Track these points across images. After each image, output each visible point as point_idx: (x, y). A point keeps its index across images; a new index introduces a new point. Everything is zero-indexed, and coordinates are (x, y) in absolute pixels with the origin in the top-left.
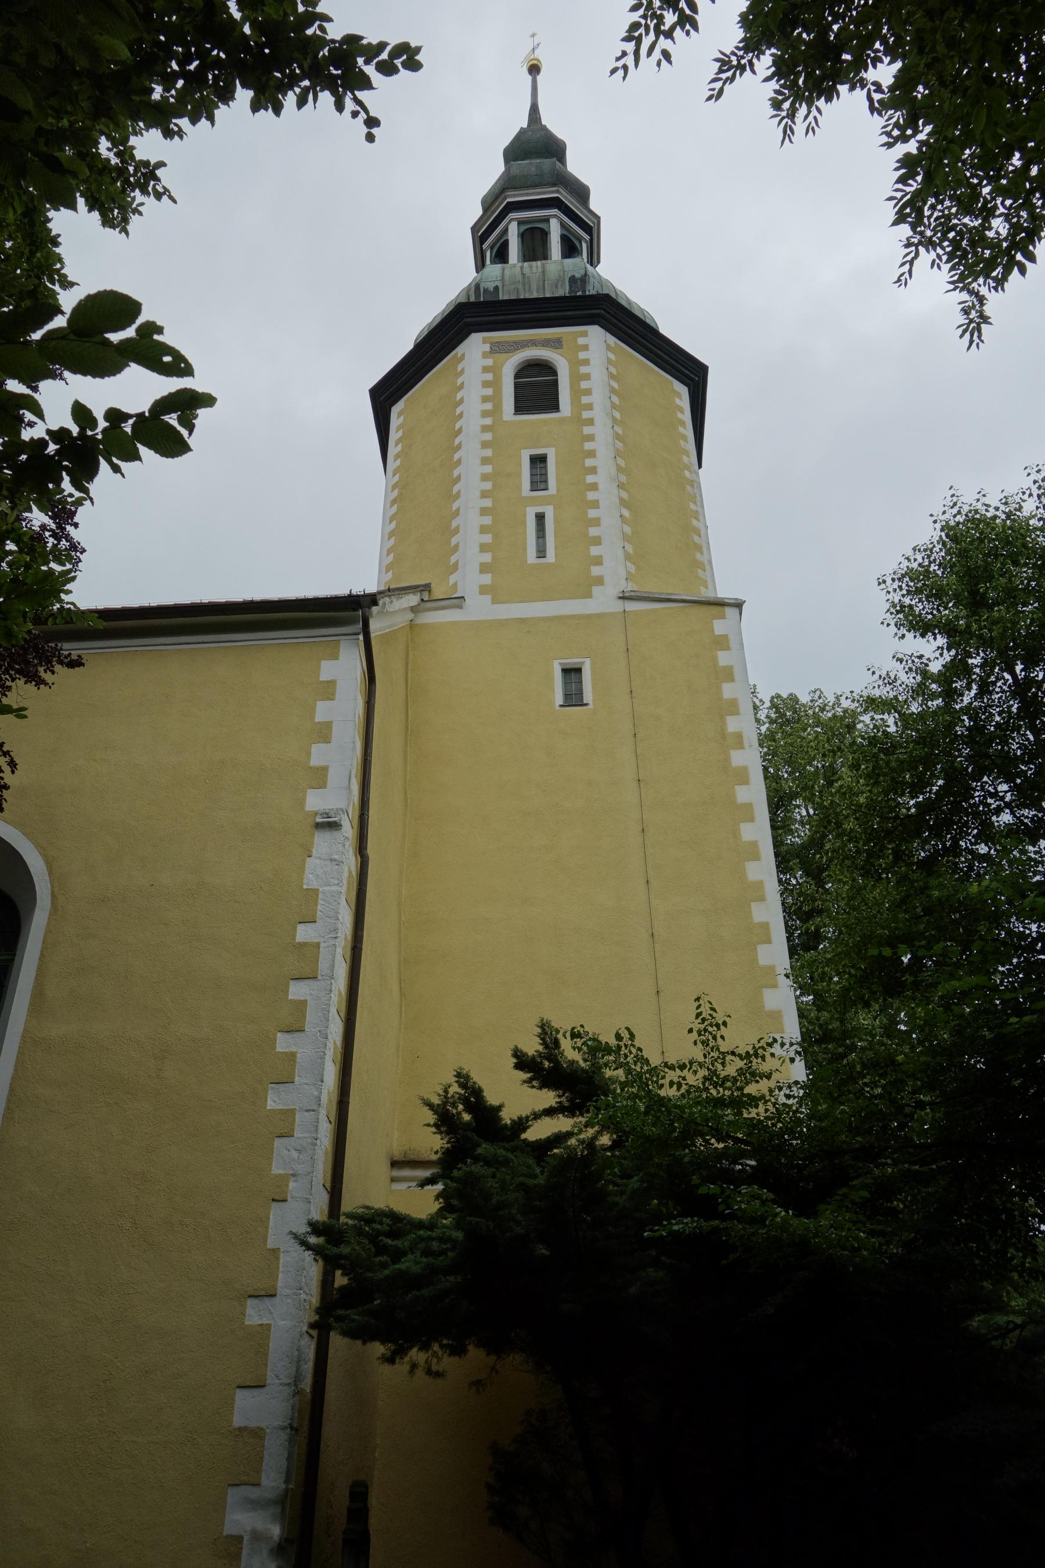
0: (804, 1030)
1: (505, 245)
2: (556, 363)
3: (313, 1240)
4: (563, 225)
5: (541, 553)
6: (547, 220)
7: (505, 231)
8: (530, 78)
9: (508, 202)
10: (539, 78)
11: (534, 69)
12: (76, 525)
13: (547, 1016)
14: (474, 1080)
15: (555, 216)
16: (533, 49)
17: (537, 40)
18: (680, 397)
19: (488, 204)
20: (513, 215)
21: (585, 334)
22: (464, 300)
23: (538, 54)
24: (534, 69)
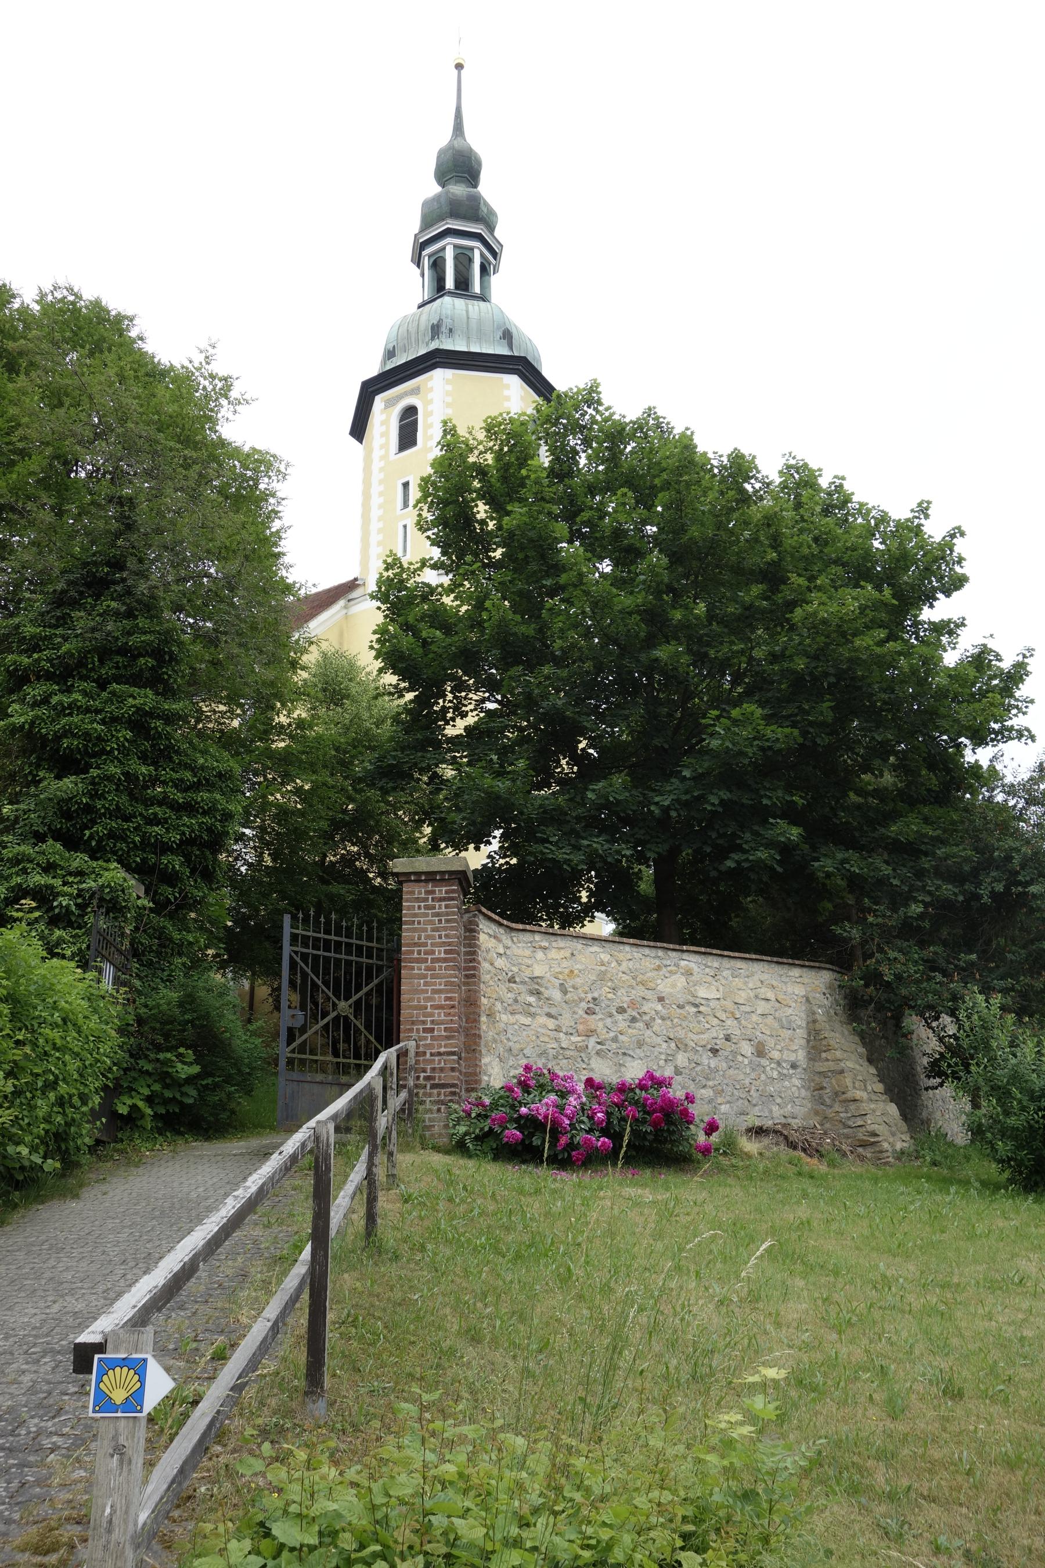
6: (443, 249)
8: (475, 140)
11: (459, 67)
20: (424, 253)
24: (459, 67)
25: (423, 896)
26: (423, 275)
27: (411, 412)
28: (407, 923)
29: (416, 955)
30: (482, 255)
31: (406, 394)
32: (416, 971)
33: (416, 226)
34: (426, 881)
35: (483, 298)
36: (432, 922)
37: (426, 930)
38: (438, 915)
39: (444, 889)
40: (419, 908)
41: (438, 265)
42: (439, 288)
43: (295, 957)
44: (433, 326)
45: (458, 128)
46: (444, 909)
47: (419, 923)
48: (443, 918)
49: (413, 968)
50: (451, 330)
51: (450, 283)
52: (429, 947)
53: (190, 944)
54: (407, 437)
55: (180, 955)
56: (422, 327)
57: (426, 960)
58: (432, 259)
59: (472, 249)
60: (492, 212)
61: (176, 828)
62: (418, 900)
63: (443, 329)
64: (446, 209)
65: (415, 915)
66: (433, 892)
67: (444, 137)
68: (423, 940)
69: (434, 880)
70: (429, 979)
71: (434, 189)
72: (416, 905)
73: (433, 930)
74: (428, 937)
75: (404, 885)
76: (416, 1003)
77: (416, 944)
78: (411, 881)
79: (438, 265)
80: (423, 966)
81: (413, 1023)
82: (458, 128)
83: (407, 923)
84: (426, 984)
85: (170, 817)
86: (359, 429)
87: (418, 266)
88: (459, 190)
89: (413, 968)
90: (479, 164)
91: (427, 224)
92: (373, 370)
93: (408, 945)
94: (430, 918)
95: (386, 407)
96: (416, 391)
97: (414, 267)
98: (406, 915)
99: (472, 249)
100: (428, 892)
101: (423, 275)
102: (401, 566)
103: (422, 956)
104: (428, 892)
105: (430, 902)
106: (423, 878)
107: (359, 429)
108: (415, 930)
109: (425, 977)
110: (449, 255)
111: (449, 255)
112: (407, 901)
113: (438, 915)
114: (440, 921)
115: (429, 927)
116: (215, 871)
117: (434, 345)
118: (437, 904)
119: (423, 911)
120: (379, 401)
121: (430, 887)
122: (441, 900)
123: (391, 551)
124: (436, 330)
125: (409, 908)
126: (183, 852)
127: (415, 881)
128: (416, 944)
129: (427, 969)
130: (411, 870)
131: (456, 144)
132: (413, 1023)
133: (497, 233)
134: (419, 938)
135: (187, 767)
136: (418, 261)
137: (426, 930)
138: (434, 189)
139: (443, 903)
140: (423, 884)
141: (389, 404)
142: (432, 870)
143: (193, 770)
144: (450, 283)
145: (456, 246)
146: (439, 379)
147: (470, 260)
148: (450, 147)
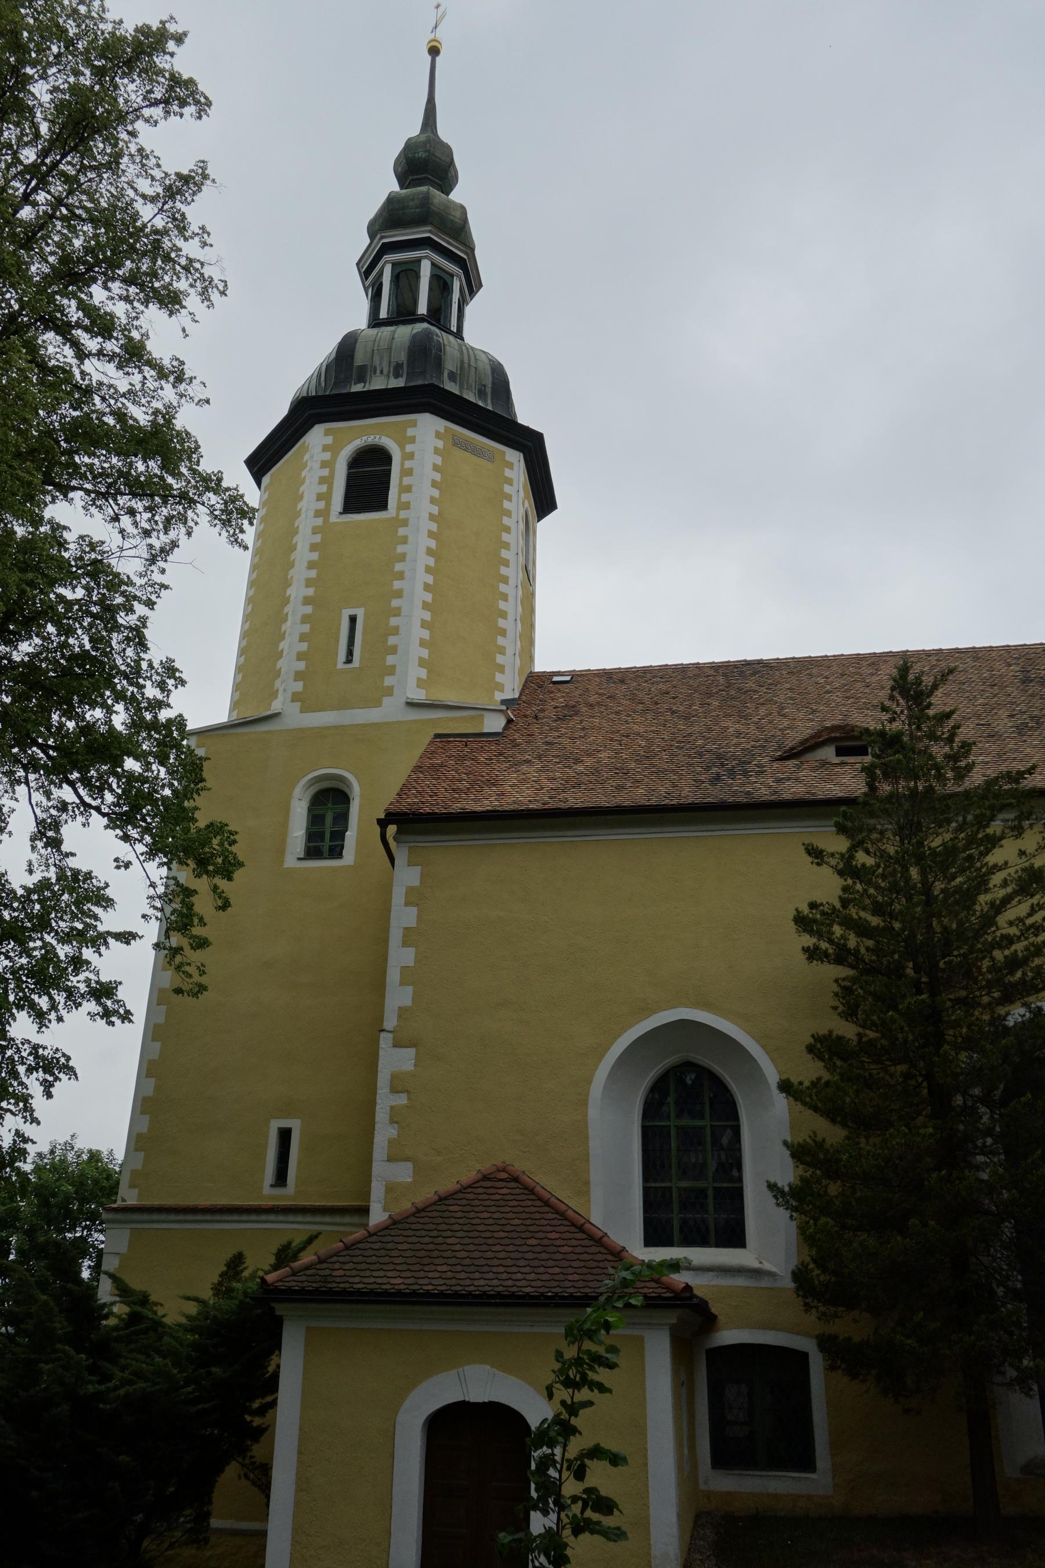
0: (735, 1173)
1: (381, 284)
2: (392, 453)
3: (106, 1310)
4: (433, 264)
5: (349, 660)
6: (418, 261)
7: (381, 274)
8: (429, 58)
9: (383, 243)
10: (438, 59)
11: (434, 51)
12: (1038, 843)
13: (594, 1407)
14: (84, 870)
15: (426, 257)
16: (436, 27)
17: (441, 10)
18: (511, 466)
19: (375, 229)
20: (387, 257)
21: (414, 424)
22: (305, 394)
23: (439, 34)
24: (434, 51)
35: (459, 335)
67: (414, 129)
110: (426, 270)
111: (426, 270)
120: (317, 437)
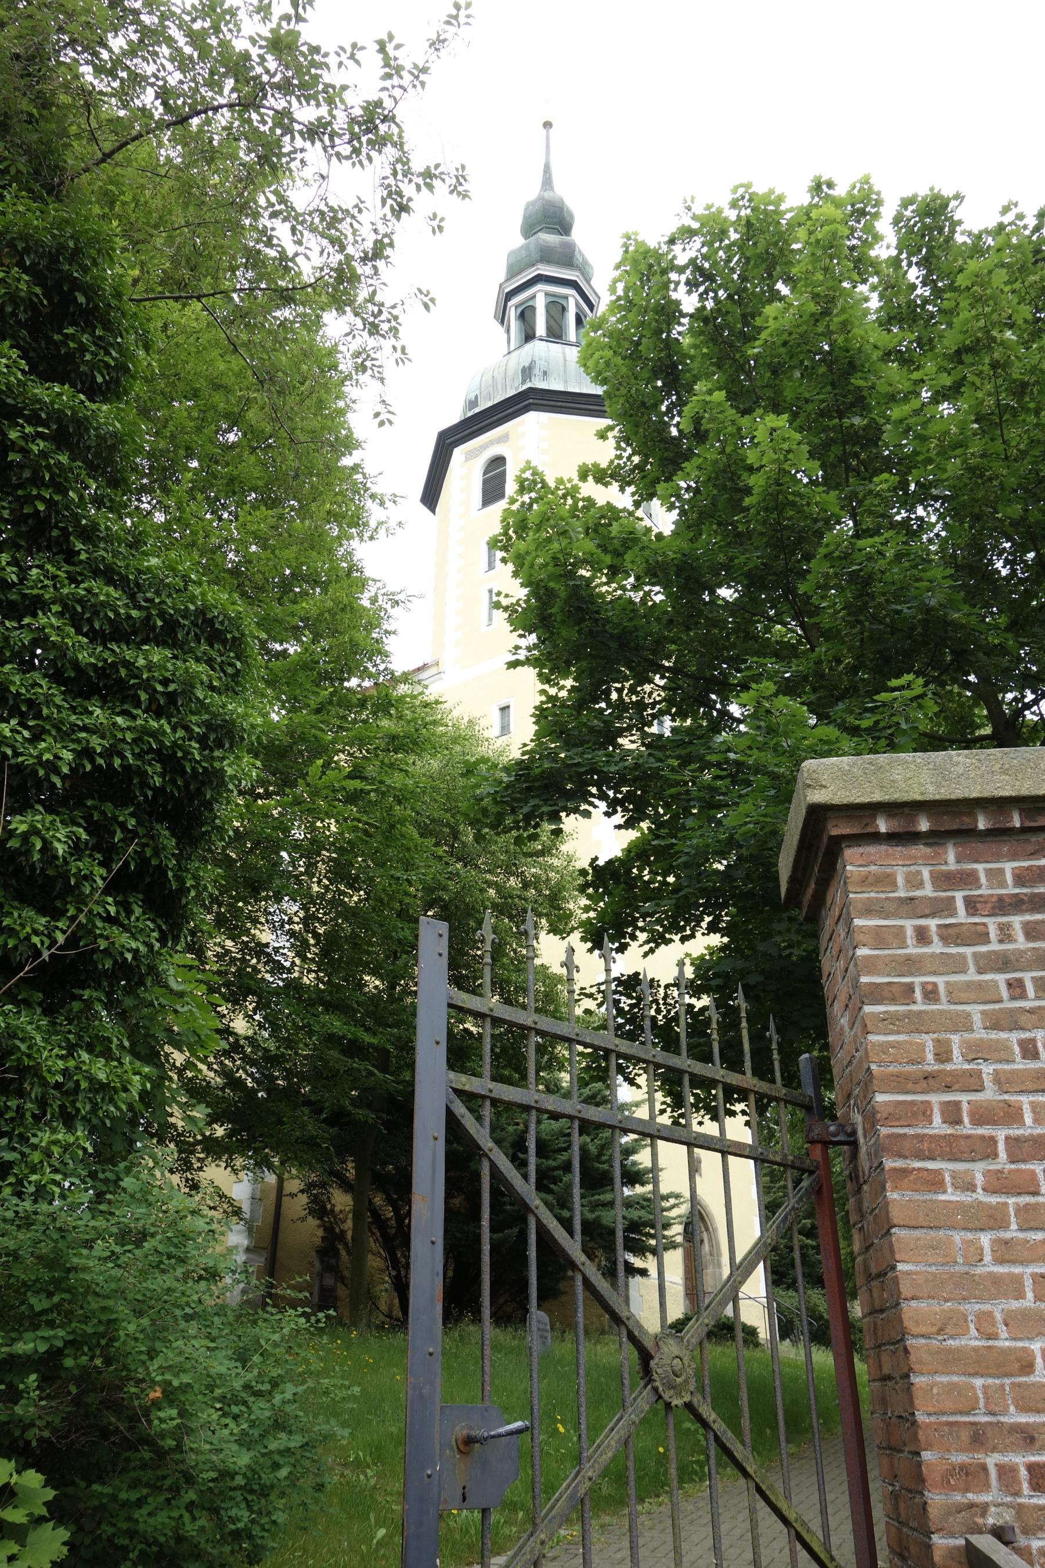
6: (533, 297)
11: (547, 125)
20: (510, 304)
25: (928, 891)
26: (508, 331)
27: (499, 461)
28: (877, 994)
29: (938, 1126)
30: (577, 305)
31: (491, 443)
32: (951, 1196)
33: (502, 276)
34: (935, 838)
36: (983, 993)
37: (963, 1024)
38: (1003, 963)
39: (1009, 867)
40: (922, 936)
41: (526, 315)
42: (529, 336)
43: (468, 1121)
44: (524, 370)
45: (547, 182)
46: (1021, 943)
47: (931, 994)
48: (1027, 977)
49: (935, 1182)
50: (545, 373)
51: (541, 329)
52: (990, 1094)
53: (102, 1087)
54: (492, 490)
55: (68, 1120)
56: (510, 373)
57: (986, 1149)
58: (519, 310)
59: (566, 298)
60: (585, 262)
61: (65, 734)
62: (910, 906)
63: (536, 371)
64: (535, 256)
65: (911, 965)
66: (968, 879)
68: (958, 1063)
69: (966, 834)
70: (1013, 1232)
71: (519, 241)
72: (909, 925)
73: (995, 1023)
74: (977, 1052)
75: (850, 853)
76: (972, 1340)
77: (929, 1080)
78: (876, 837)
79: (526, 315)
80: (978, 1171)
81: (978, 1438)
82: (547, 182)
83: (877, 994)
84: (1005, 1251)
85: (49, 701)
86: (431, 496)
87: (502, 323)
88: (550, 239)
89: (935, 1182)
90: (572, 217)
91: (512, 274)
92: (453, 416)
93: (899, 1083)
94: (972, 975)
95: (467, 460)
96: (504, 439)
97: (498, 325)
98: (871, 965)
99: (566, 298)
100: (946, 880)
101: (508, 331)
102: (545, 485)
103: (967, 1128)
104: (946, 880)
105: (962, 916)
106: (924, 825)
107: (431, 496)
108: (917, 1023)
109: (995, 1220)
112: (869, 911)
113: (1003, 963)
114: (1016, 988)
115: (975, 1011)
116: (183, 891)
117: (528, 385)
118: (992, 924)
119: (937, 947)
120: (459, 454)
121: (951, 857)
122: (1003, 906)
123: (528, 462)
124: (527, 372)
125: (879, 938)
126: (88, 818)
127: (893, 838)
128: (929, 1080)
129: (999, 1184)
130: (877, 797)
131: (547, 195)
132: (978, 1438)
133: (592, 283)
134: (943, 1055)
135: (109, 575)
136: (502, 318)
137: (963, 1024)
138: (519, 241)
139: (1016, 921)
140: (921, 850)
141: (471, 456)
142: (959, 792)
143: (132, 590)
144: (541, 329)
145: (547, 294)
146: (533, 421)
147: (564, 309)
148: (540, 198)
